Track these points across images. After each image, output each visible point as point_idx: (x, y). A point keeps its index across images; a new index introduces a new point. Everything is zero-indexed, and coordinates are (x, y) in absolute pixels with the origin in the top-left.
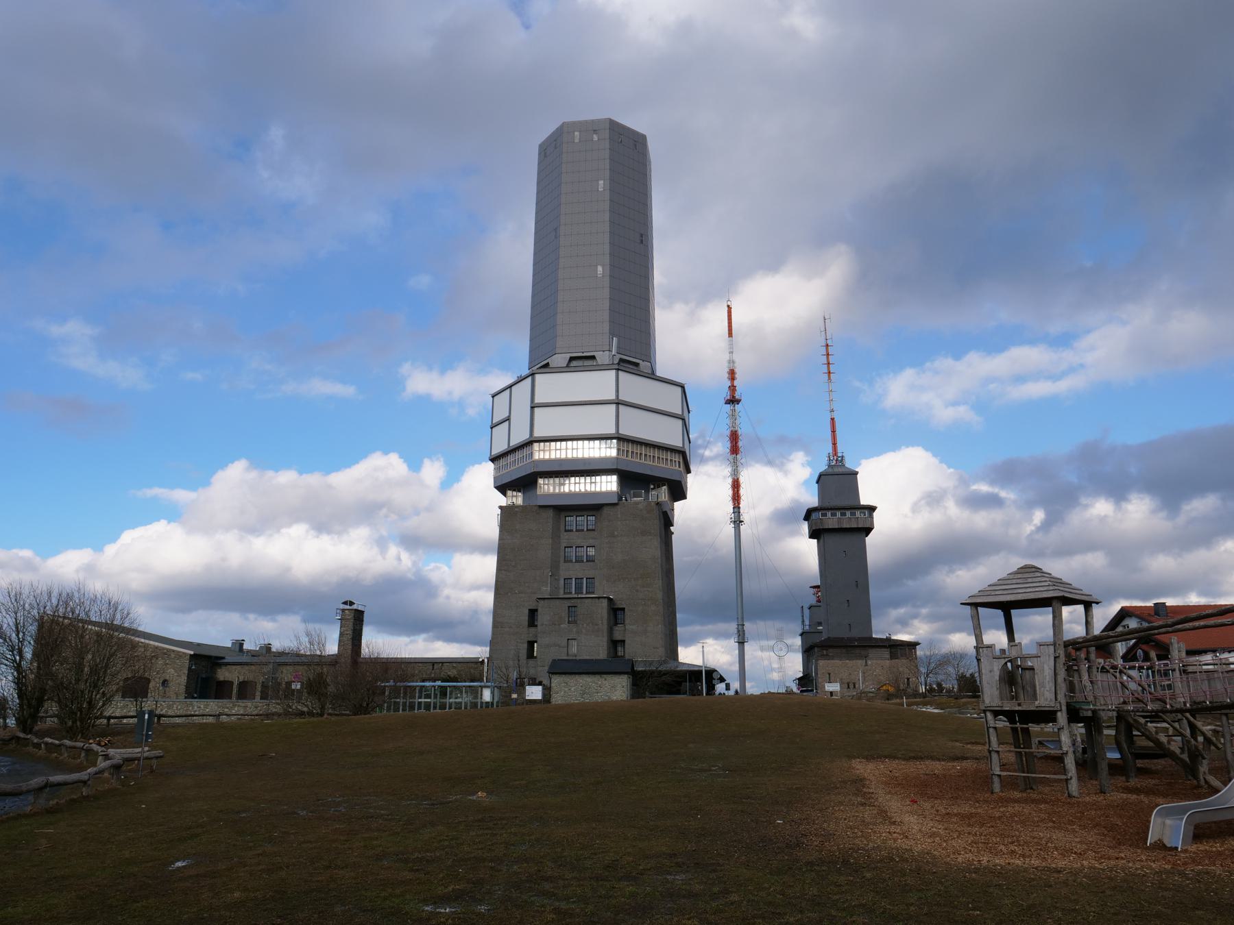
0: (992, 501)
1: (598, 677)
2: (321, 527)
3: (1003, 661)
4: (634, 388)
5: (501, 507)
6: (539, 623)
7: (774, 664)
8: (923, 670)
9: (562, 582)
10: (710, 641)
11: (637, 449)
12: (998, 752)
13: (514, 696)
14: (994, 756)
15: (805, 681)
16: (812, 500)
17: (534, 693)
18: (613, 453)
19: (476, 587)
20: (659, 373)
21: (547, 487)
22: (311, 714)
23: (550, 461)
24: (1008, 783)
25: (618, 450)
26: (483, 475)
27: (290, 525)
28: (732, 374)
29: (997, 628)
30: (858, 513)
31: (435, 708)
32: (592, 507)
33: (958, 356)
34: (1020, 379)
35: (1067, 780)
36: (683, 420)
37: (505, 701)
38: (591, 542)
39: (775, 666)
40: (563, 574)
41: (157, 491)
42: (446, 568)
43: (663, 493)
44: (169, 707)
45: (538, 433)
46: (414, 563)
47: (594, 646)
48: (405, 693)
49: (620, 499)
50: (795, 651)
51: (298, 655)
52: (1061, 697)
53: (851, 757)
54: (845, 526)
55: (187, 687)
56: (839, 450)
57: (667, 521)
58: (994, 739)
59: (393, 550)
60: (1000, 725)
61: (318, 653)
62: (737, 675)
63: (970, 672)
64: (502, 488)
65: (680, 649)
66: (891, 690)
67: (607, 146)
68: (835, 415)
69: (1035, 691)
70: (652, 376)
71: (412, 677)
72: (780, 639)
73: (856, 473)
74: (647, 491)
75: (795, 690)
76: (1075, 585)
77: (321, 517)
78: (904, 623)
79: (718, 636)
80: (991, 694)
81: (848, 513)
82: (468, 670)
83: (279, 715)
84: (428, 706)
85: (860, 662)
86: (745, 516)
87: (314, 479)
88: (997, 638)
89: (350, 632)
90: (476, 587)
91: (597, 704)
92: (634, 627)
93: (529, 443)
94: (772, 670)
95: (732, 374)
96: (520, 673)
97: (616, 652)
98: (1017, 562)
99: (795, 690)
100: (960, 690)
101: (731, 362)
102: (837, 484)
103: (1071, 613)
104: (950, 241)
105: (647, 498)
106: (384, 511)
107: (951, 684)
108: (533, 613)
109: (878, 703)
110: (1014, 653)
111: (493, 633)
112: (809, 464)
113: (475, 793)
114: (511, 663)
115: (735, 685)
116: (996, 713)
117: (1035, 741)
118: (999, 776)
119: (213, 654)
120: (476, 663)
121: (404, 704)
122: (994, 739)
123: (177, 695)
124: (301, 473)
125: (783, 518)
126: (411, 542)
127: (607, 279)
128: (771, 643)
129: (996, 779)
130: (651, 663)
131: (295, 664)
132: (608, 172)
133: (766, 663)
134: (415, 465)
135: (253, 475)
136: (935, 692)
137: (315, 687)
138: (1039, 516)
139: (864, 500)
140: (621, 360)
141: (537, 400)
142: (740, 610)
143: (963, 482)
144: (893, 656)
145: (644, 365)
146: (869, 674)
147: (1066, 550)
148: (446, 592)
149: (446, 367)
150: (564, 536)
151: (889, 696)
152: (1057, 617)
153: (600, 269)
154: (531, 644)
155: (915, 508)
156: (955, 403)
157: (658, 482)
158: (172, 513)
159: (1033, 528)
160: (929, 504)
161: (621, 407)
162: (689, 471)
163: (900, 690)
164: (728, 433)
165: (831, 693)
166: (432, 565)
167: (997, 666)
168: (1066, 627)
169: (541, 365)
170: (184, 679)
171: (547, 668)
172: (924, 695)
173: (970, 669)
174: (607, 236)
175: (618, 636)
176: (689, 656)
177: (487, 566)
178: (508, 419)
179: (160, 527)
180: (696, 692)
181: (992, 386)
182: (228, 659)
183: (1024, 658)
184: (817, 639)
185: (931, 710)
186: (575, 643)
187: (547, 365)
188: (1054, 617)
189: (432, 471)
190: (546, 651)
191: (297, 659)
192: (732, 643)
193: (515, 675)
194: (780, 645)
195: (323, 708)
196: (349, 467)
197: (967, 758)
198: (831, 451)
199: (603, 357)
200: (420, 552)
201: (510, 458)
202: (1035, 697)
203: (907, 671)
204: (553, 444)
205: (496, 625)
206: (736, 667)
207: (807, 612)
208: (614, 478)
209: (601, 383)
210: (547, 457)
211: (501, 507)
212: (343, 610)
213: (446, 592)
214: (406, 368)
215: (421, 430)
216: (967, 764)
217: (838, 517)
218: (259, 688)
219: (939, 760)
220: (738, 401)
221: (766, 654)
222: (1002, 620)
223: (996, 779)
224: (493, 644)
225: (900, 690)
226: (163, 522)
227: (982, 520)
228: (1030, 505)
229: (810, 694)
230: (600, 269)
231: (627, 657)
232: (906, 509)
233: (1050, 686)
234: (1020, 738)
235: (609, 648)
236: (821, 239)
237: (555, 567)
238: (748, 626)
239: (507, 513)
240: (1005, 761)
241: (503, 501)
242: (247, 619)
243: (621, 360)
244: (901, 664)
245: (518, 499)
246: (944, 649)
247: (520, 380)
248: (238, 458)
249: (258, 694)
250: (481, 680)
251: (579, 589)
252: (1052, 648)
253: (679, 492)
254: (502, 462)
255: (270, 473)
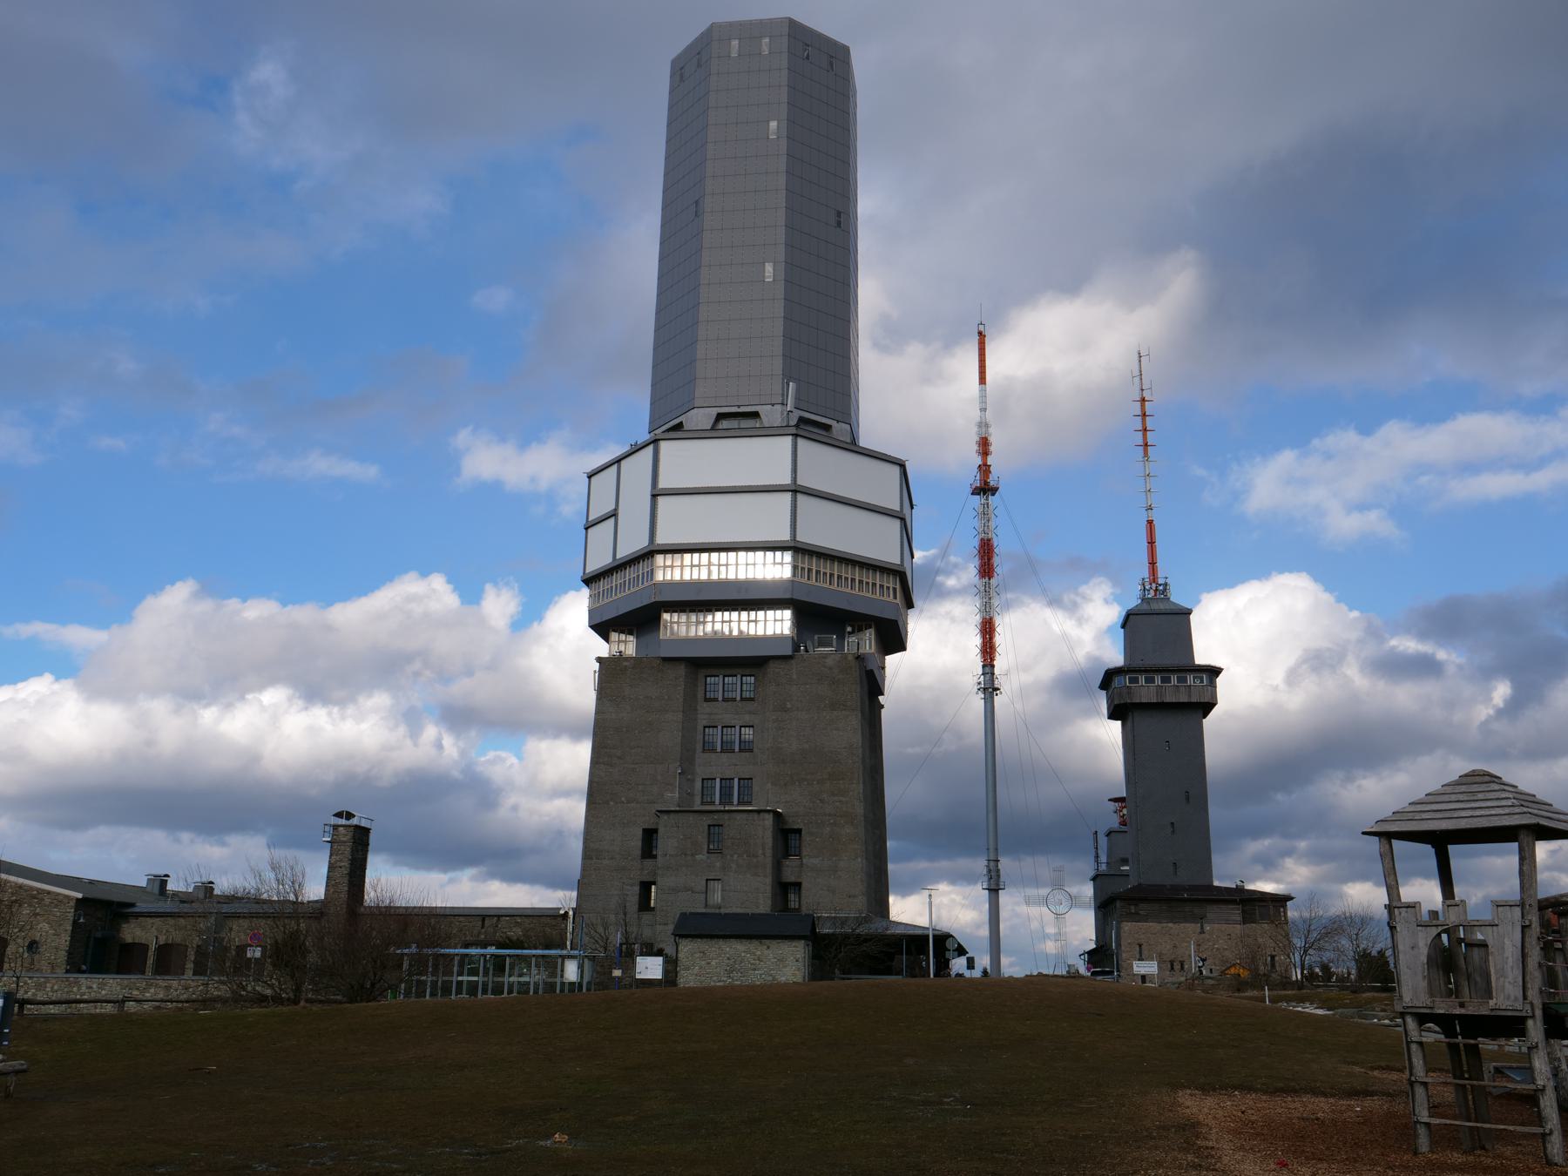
0: (1425, 667)
1: (756, 942)
2: (313, 692)
3: (1434, 931)
4: (824, 466)
5: (599, 660)
6: (659, 852)
7: (1047, 927)
8: (1298, 943)
9: (698, 785)
10: (943, 887)
11: (826, 567)
12: (1425, 1084)
13: (617, 973)
14: (1420, 1091)
15: (1099, 956)
16: (1115, 656)
17: (650, 968)
18: (786, 572)
19: (566, 793)
20: (864, 442)
21: (678, 626)
22: (277, 1000)
23: (682, 584)
24: (1442, 1139)
25: (795, 568)
26: (572, 614)
27: (262, 687)
28: (984, 446)
29: (1427, 876)
30: (1190, 679)
31: (485, 991)
32: (750, 662)
33: (1366, 429)
34: (1470, 467)
35: (1544, 1135)
36: (903, 520)
37: (600, 980)
38: (747, 719)
39: (1051, 930)
40: (701, 771)
41: (38, 628)
42: (513, 760)
43: (867, 642)
44: (39, 987)
45: (662, 539)
46: (463, 753)
47: (749, 892)
48: (436, 967)
49: (796, 648)
50: (1082, 906)
51: (258, 901)
52: (1533, 994)
53: (1176, 1086)
54: (1168, 700)
55: (70, 953)
56: (1161, 574)
57: (873, 685)
58: (1418, 1062)
59: (430, 732)
60: (1429, 1038)
61: (292, 897)
62: (986, 944)
63: (1378, 947)
64: (602, 628)
65: (891, 899)
66: (1244, 974)
67: (785, 64)
68: (1154, 515)
69: (1489, 982)
70: (852, 446)
71: (447, 941)
72: (1058, 885)
73: (1189, 612)
74: (841, 637)
75: (1083, 970)
76: (1557, 806)
77: (383, 688)
78: (1268, 864)
79: (956, 878)
80: (1413, 986)
81: (1174, 679)
82: (541, 929)
83: (224, 1001)
84: (473, 988)
85: (1192, 928)
86: (1000, 681)
87: (304, 614)
88: (1424, 891)
89: (346, 864)
90: (566, 793)
91: (752, 987)
92: (816, 861)
93: (648, 555)
94: (1045, 937)
95: (984, 446)
96: (626, 934)
97: (786, 900)
98: (1460, 766)
99: (1083, 970)
100: (1360, 977)
101: (983, 424)
102: (1157, 629)
103: (1553, 853)
104: (1352, 246)
105: (840, 647)
106: (417, 665)
107: (1345, 967)
108: (650, 835)
109: (1222, 997)
110: (1453, 918)
111: (584, 868)
112: (1117, 599)
113: (550, 1136)
114: (612, 917)
115: (983, 961)
116: (1422, 1019)
117: (1489, 1067)
118: (1427, 1125)
119: (115, 898)
120: (554, 917)
121: (434, 983)
122: (1418, 1062)
123: (53, 967)
124: (284, 603)
125: (1069, 686)
126: (458, 717)
127: (781, 286)
128: (1044, 891)
129: (1422, 1131)
130: (844, 921)
131: (252, 916)
132: (784, 107)
133: (1035, 925)
134: (470, 594)
135: (206, 606)
136: (1318, 981)
137: (286, 954)
138: (1502, 691)
139: (1201, 658)
140: (802, 420)
141: (662, 484)
142: (992, 834)
143: (1374, 633)
144: (1247, 919)
145: (839, 429)
146: (1208, 944)
147: (1542, 750)
148: (512, 800)
149: (528, 437)
150: (704, 708)
151: (1240, 985)
152: (1527, 858)
153: (769, 268)
154: (645, 887)
155: (1292, 677)
156: (1362, 507)
157: (859, 621)
158: (63, 665)
159: (1491, 712)
160: (1316, 669)
161: (799, 496)
162: (910, 605)
163: (1260, 975)
164: (976, 543)
165: (1144, 977)
166: (491, 755)
167: (1424, 939)
168: (1542, 876)
169: (669, 426)
170: (65, 940)
171: (671, 927)
172: (1299, 985)
173: (1379, 942)
174: (782, 214)
175: (789, 876)
176: (906, 910)
177: (572, 760)
178: (614, 514)
179: (38, 687)
180: (917, 971)
181: (1424, 479)
182: (141, 907)
183: (1469, 927)
184: (1120, 887)
185: (1311, 1009)
186: (718, 886)
187: (679, 427)
188: (1522, 859)
189: (499, 605)
190: (671, 898)
191: (255, 908)
192: (979, 892)
193: (617, 938)
194: (1059, 895)
195: (298, 990)
196: (365, 594)
197: (1372, 1094)
198: (1146, 574)
199: (772, 415)
200: (473, 733)
201: (617, 579)
202: (1488, 993)
203: (1271, 943)
204: (687, 556)
205: (588, 854)
206: (985, 932)
207: (1103, 842)
208: (788, 614)
209: (767, 458)
210: (677, 577)
211: (599, 660)
212: (335, 827)
213: (1103, 867)
214: (463, 437)
215: (481, 538)
216: (1375, 1104)
217: (1157, 684)
218: (192, 956)
219: (1325, 1095)
220: (994, 491)
221: (1034, 911)
222: (1432, 863)
223: (1422, 1131)
224: (582, 886)
225: (1260, 975)
226: (48, 678)
227: (1405, 697)
228: (1487, 674)
229: (1108, 978)
230: (769, 268)
231: (804, 911)
232: (1278, 676)
233: (1514, 974)
234: (1463, 1062)
235: (774, 895)
236: (1152, 241)
237: (687, 760)
238: (1005, 864)
239: (608, 668)
240: (1437, 1100)
241: (602, 648)
242: (178, 841)
243: (802, 420)
244: (1261, 931)
245: (628, 646)
246: (1335, 909)
247: (636, 449)
248: (181, 577)
249: (190, 966)
250: (563, 946)
251: (726, 796)
252: (1518, 911)
253: (894, 640)
254: (603, 585)
255: (233, 603)
